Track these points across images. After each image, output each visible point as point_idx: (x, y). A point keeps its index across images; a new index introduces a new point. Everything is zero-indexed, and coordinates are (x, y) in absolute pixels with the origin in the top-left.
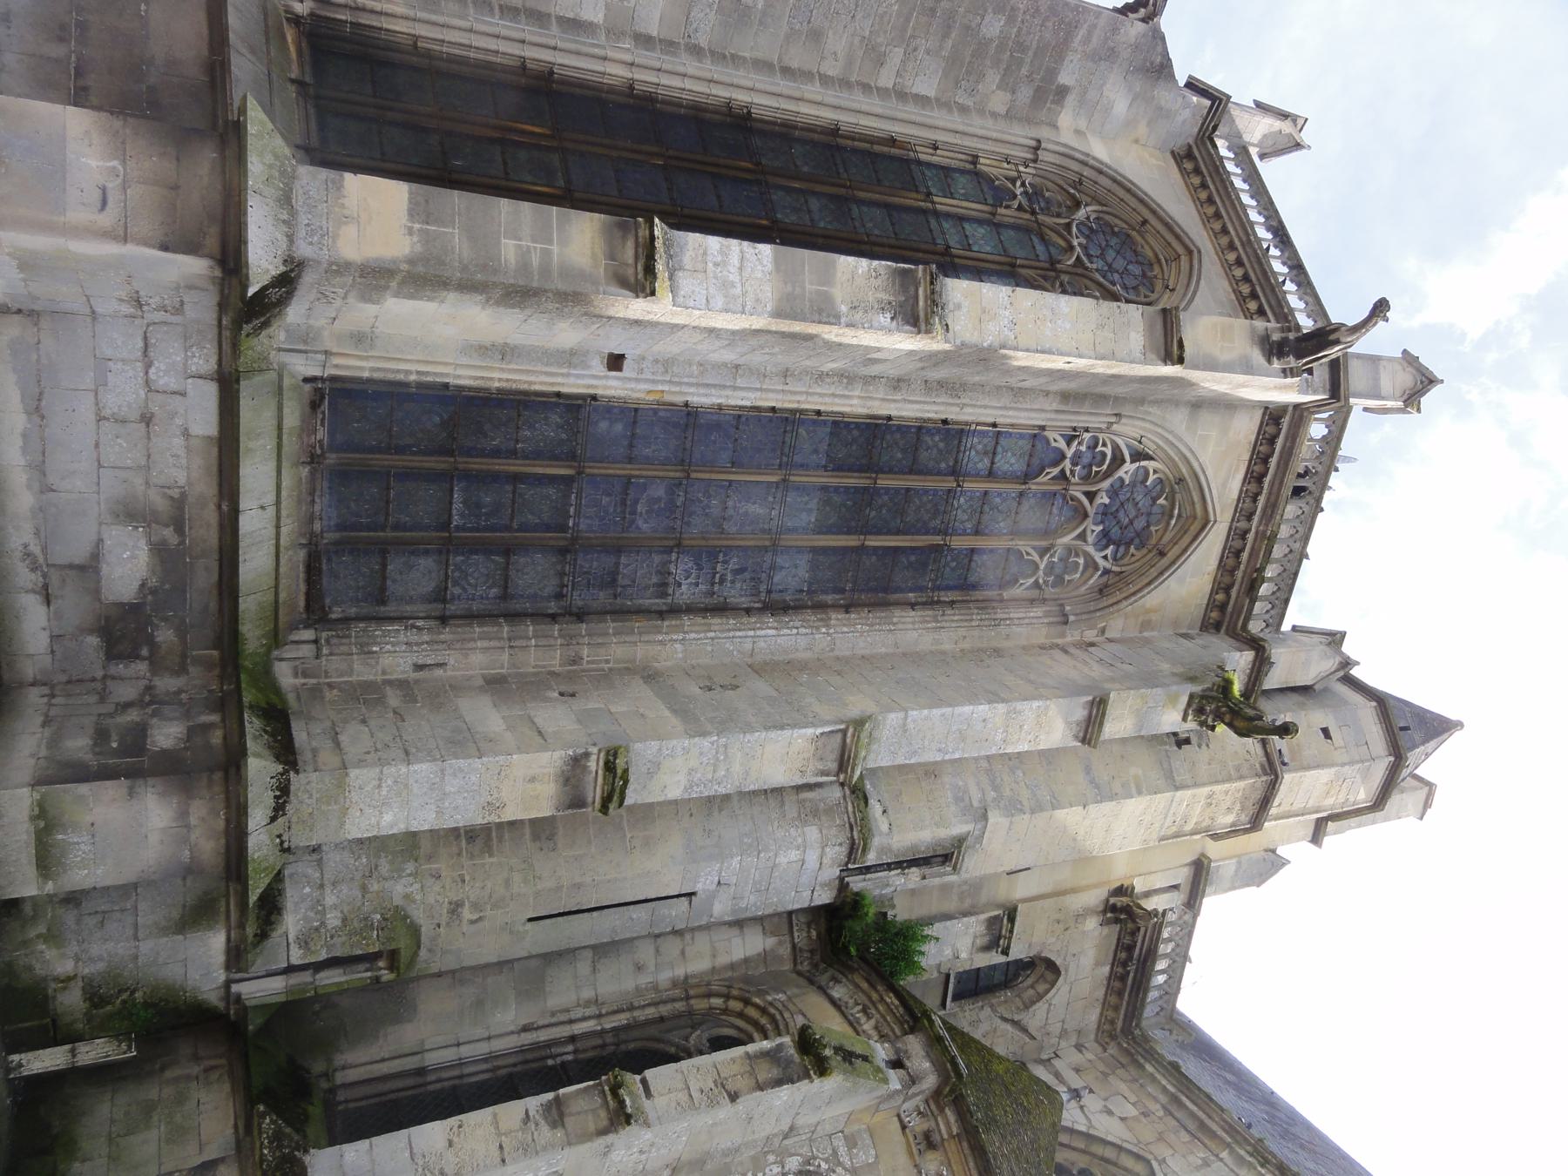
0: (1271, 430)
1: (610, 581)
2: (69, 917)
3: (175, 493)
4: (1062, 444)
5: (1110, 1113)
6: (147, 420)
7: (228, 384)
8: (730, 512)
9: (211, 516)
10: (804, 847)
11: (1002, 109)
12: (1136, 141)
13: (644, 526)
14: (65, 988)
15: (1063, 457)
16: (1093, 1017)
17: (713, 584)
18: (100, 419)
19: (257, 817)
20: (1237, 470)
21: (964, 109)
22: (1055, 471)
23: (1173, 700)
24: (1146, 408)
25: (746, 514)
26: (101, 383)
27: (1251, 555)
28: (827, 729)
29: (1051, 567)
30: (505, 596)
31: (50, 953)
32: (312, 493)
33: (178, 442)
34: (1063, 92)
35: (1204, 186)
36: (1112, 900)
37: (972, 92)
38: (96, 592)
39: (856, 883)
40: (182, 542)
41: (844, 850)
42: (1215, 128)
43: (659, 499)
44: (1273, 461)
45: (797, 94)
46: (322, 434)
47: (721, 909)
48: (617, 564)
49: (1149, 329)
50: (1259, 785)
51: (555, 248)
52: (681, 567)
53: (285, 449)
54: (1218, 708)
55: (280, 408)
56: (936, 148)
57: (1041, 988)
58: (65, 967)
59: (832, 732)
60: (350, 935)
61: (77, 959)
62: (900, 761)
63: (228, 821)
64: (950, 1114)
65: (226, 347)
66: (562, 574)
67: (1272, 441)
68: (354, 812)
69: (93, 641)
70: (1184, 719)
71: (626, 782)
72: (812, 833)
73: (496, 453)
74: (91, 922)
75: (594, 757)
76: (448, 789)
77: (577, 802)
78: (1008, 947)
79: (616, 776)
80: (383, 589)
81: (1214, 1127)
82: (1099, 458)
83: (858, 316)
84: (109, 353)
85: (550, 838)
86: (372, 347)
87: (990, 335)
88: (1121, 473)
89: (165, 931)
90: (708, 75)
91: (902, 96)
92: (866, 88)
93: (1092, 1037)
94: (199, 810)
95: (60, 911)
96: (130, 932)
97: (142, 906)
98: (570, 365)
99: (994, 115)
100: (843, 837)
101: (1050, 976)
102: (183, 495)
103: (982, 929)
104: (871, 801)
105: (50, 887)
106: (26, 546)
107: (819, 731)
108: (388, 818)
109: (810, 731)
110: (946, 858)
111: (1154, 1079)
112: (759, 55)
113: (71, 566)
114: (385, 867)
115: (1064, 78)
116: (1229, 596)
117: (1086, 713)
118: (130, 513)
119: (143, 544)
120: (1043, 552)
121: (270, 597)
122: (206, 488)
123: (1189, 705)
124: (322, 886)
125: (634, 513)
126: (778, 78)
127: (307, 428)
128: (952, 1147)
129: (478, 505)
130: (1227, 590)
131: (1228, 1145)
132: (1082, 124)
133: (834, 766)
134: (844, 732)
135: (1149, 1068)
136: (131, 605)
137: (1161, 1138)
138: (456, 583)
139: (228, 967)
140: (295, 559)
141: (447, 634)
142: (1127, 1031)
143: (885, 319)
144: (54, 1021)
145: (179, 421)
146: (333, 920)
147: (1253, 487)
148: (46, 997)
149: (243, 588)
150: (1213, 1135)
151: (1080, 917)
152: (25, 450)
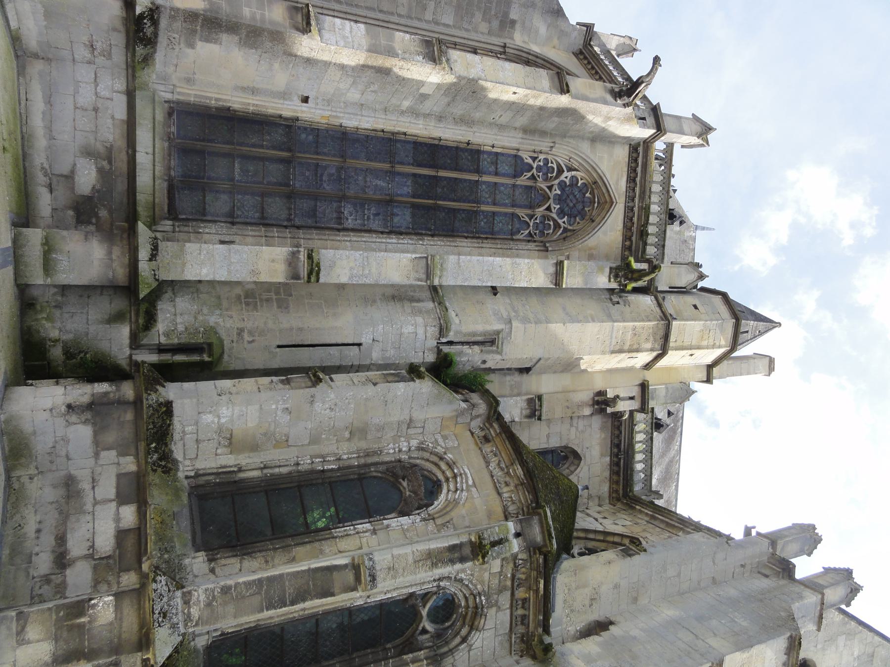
0: (635, 155)
1: (313, 213)
2: (57, 313)
3: (108, 145)
4: (530, 161)
5: (616, 524)
6: (96, 110)
7: (130, 95)
8: (369, 184)
9: (124, 157)
10: (416, 325)
11: (486, 31)
12: (554, 47)
13: (327, 188)
14: (54, 346)
15: (532, 168)
16: (605, 488)
17: (364, 220)
18: (76, 108)
19: (144, 254)
20: (622, 176)
21: (467, 30)
22: (529, 174)
23: (601, 270)
24: (567, 139)
25: (376, 185)
26: (76, 92)
27: (638, 219)
28: (418, 256)
29: (536, 226)
30: (263, 218)
31: (48, 325)
32: (170, 155)
33: (110, 121)
34: (513, 22)
35: (589, 63)
36: (596, 398)
37: (470, 23)
38: (72, 189)
39: (446, 349)
40: (111, 169)
41: (437, 329)
42: (590, 40)
43: (333, 175)
44: (639, 169)
45: (387, 19)
46: (173, 129)
47: (376, 356)
48: (316, 206)
49: (551, 79)
50: (660, 326)
51: (267, 13)
52: (347, 210)
53: (156, 130)
54: (625, 274)
55: (154, 110)
56: (456, 45)
57: (572, 468)
58: (54, 334)
59: (421, 257)
60: (189, 334)
61: (60, 330)
62: (459, 283)
63: (130, 259)
64: (496, 425)
65: (130, 78)
66: (290, 209)
67: (636, 160)
68: (188, 266)
69: (71, 213)
70: (610, 281)
71: (319, 270)
72: (419, 320)
73: (254, 146)
74: (66, 315)
75: (302, 253)
76: (232, 260)
77: (296, 277)
78: (541, 415)
79: (314, 271)
80: (204, 209)
81: (673, 523)
82: (551, 170)
83: (407, 56)
84: (80, 79)
85: (286, 308)
86: (194, 84)
87: (473, 74)
88: (562, 178)
89: (101, 322)
90: (345, 10)
91: (437, 23)
92: (419, 20)
93: (607, 501)
94: (117, 251)
95: (53, 310)
96: (85, 321)
97: (90, 312)
98: (284, 99)
99: (482, 33)
100: (436, 323)
101: (576, 462)
102: (112, 146)
103: (525, 405)
104: (449, 310)
105: (49, 281)
106: (42, 164)
107: (414, 256)
108: (204, 271)
109: (409, 255)
110: (492, 342)
111: (641, 512)
112: (368, 5)
113: (62, 176)
114: (205, 311)
115: (513, 16)
116: (632, 242)
117: (554, 269)
118: (88, 153)
119: (93, 167)
120: (531, 217)
121: (151, 199)
122: (121, 143)
123: (610, 273)
124: (175, 315)
125: (321, 180)
126: (378, 13)
127: (167, 125)
128: (497, 440)
129: (248, 171)
130: (630, 239)
131: (681, 529)
132: (526, 39)
133: (424, 276)
134: (427, 258)
135: (638, 507)
136: (88, 196)
137: (644, 530)
138: (238, 209)
139: (131, 348)
140: (162, 186)
141: (235, 229)
142: (626, 495)
143: (420, 58)
144: (49, 363)
145: (110, 112)
146: (181, 328)
147: (632, 185)
148: (45, 348)
149: (138, 189)
150: (674, 526)
151: (580, 406)
152: (43, 120)
